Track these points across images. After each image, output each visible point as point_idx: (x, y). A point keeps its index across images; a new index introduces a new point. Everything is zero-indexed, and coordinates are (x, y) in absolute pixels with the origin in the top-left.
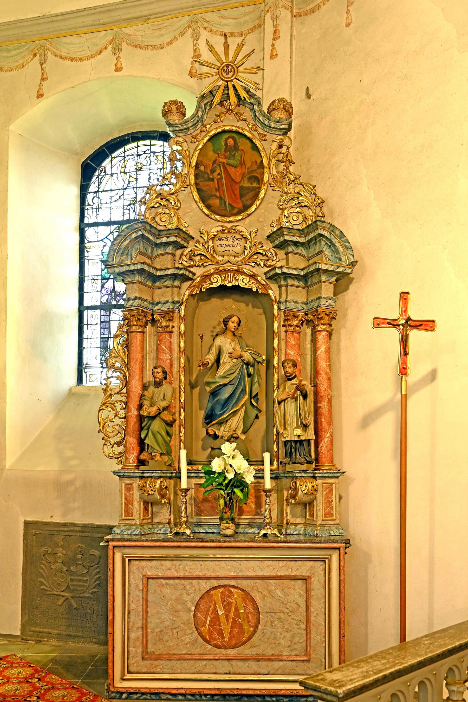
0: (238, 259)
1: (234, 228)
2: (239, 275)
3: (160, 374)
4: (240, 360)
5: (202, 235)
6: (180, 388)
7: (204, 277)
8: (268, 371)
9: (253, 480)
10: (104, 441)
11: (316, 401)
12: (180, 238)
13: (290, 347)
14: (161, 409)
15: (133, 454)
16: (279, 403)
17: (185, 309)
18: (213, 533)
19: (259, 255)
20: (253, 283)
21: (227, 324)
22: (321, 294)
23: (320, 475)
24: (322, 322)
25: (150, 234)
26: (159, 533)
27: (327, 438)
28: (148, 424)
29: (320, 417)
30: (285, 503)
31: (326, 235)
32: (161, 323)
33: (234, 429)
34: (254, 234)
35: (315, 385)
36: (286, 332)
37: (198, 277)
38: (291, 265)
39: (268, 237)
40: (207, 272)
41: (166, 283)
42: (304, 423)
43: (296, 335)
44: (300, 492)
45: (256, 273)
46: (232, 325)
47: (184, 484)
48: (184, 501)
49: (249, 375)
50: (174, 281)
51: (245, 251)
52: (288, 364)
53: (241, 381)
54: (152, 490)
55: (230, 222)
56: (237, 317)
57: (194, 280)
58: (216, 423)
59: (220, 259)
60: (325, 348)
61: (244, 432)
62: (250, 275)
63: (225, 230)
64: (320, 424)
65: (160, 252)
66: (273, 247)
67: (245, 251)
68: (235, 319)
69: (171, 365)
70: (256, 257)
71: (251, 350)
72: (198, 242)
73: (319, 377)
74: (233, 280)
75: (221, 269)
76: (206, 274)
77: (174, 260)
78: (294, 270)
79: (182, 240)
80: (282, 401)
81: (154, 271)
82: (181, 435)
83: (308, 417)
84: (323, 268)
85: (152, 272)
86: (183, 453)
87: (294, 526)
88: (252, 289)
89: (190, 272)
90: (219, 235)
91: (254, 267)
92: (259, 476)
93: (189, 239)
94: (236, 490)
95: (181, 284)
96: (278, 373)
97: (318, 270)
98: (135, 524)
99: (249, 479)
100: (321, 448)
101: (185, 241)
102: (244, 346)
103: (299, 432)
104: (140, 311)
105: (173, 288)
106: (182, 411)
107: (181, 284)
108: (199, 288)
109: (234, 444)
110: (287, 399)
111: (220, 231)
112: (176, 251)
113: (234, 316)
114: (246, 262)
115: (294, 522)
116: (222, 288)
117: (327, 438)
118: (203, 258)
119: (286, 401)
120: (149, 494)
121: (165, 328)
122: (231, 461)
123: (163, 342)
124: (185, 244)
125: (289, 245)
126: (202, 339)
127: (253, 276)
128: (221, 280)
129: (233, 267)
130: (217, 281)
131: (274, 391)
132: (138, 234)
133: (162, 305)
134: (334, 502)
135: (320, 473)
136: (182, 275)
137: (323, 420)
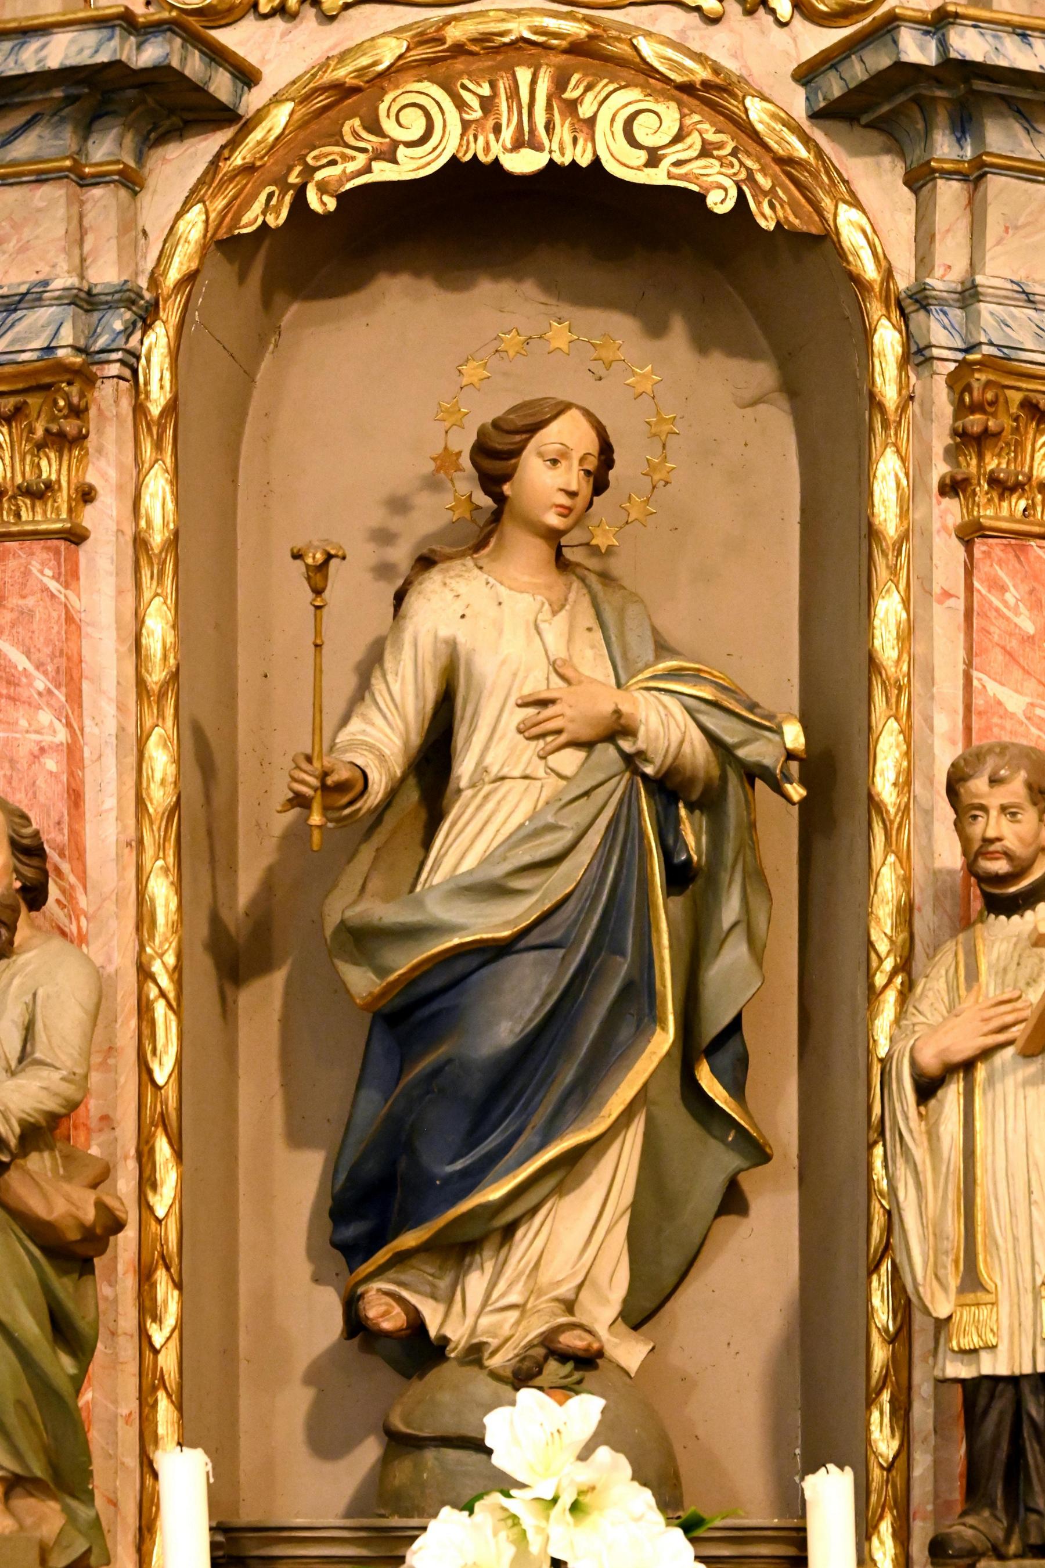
2: (603, 87)
4: (607, 754)
6: (144, 973)
7: (321, 101)
13: (997, 657)
16: (927, 1088)
17: (175, 354)
20: (706, 151)
21: (507, 477)
36: (971, 534)
37: (277, 100)
40: (343, 57)
41: (23, 148)
45: (731, 65)
46: (544, 479)
49: (680, 876)
50: (86, 128)
52: (995, 781)
56: (588, 414)
57: (248, 126)
61: (638, 1315)
62: (687, 88)
68: (570, 433)
71: (696, 677)
74: (549, 127)
75: (454, 34)
76: (342, 73)
86: (185, 1479)
88: (701, 198)
89: (218, 55)
95: (140, 158)
96: (905, 860)
102: (643, 648)
105: (85, 182)
106: (163, 1149)
107: (140, 158)
108: (285, 187)
109: (586, 1410)
110: (987, 1053)
113: (562, 408)
119: (981, 1072)
126: (318, 592)
127: (711, 95)
128: (455, 127)
129: (553, 24)
130: (421, 137)
131: (873, 995)
136: (162, 76)
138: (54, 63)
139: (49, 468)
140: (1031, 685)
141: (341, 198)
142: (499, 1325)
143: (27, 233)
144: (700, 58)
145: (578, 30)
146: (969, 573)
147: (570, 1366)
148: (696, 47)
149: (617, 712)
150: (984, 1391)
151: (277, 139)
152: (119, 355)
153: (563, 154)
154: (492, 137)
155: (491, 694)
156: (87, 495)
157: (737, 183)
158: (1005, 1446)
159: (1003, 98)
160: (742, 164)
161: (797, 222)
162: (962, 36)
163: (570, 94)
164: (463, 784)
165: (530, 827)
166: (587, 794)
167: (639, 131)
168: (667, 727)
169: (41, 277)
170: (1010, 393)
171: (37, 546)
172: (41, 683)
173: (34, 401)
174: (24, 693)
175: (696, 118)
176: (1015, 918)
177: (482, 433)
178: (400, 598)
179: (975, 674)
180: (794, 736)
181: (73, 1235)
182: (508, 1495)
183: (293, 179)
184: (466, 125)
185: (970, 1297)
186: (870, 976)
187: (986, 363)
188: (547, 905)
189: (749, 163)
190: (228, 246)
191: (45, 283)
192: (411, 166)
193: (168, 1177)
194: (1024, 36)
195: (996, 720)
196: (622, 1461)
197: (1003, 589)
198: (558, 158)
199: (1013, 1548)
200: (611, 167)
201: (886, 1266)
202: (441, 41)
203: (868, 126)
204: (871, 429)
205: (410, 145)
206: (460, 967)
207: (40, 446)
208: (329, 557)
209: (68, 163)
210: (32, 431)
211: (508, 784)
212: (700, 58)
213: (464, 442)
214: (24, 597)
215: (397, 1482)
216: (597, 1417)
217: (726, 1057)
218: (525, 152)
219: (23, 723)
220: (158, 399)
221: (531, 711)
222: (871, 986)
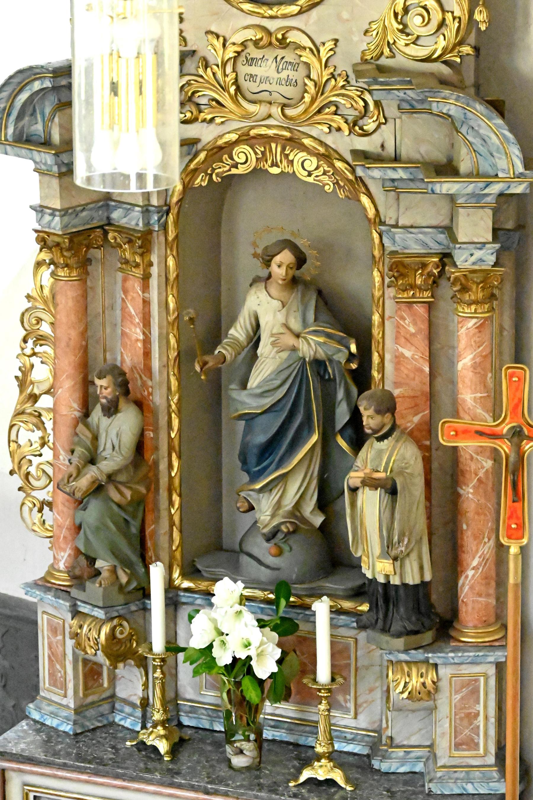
2: (296, 151)
3: (109, 390)
6: (170, 406)
8: (431, 313)
10: (22, 494)
13: (403, 340)
15: (64, 550)
27: (473, 568)
29: (459, 517)
51: (306, 95)
60: (473, 359)
64: (459, 534)
67: (306, 95)
69: (147, 354)
74: (281, 161)
76: (220, 142)
82: (173, 511)
90: (248, 51)
108: (207, 174)
117: (473, 568)
128: (254, 160)
134: (481, 718)
137: (465, 527)
140: (413, 348)
141: (222, 178)
145: (287, 134)
155: (264, 331)
156: (151, 264)
157: (334, 184)
160: (335, 178)
163: (287, 152)
167: (306, 164)
172: (137, 320)
175: (322, 162)
183: (209, 172)
184: (257, 159)
193: (176, 463)
195: (402, 359)
197: (404, 319)
202: (249, 135)
205: (241, 164)
218: (275, 168)
220: (170, 238)
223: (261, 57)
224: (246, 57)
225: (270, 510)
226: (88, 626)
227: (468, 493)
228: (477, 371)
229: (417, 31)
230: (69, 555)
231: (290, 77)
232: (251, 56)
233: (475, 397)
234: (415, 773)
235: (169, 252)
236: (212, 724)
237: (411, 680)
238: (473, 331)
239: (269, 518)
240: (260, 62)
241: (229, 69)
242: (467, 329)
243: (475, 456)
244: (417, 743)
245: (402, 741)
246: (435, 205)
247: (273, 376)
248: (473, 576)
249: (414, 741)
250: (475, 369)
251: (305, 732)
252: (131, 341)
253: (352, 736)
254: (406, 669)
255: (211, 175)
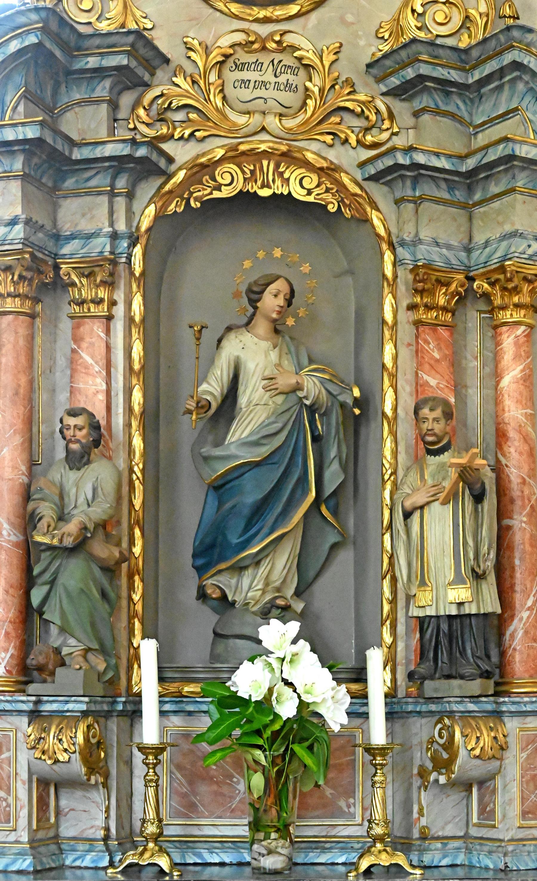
0: (290, 123)
1: (277, 38)
2: (292, 168)
3: (84, 431)
4: (293, 398)
5: (191, 54)
6: (131, 471)
7: (195, 170)
9: (345, 720)
11: (502, 513)
12: (136, 58)
13: (427, 367)
14: (91, 526)
17: (144, 255)
18: (222, 864)
19: (347, 116)
20: (327, 190)
21: (259, 300)
22: (513, 224)
23: (513, 708)
24: (516, 299)
25: (58, 44)
26: (80, 868)
27: (528, 609)
28: (53, 569)
30: (417, 782)
31: (531, 66)
32: (80, 290)
33: (277, 584)
34: (333, 57)
35: (498, 469)
36: (418, 323)
38: (430, 146)
39: (369, 66)
40: (204, 155)
41: (93, 183)
42: (477, 570)
43: (443, 332)
44: (462, 753)
45: (335, 161)
46: (271, 301)
47: (150, 731)
48: (151, 781)
49: (316, 439)
52: (431, 410)
53: (298, 451)
54: (66, 750)
55: (266, 20)
56: (287, 280)
57: (170, 177)
58: (227, 569)
59: (242, 120)
60: (522, 371)
61: (298, 593)
62: (321, 169)
63: (253, 43)
64: (508, 573)
65: (78, 96)
66: (383, 94)
67: (309, 101)
68: (279, 285)
70: (338, 120)
71: (323, 371)
72: (179, 70)
73: (505, 448)
74: (274, 181)
75: (242, 148)
76: (203, 160)
77: (115, 120)
78: (443, 159)
79: (140, 64)
80: (415, 509)
81: (66, 147)
83: (488, 554)
84: (523, 155)
85: (59, 147)
86: (148, 649)
87: (439, 845)
88: (325, 207)
89: (162, 153)
90: (237, 56)
91: (331, 146)
92: (358, 713)
93: (156, 62)
94: (297, 748)
97: (511, 157)
98: (17, 842)
99: (336, 717)
100: (512, 636)
101: (145, 68)
102: (305, 361)
103: (461, 593)
104: (27, 256)
106: (137, 532)
108: (183, 199)
109: (294, 627)
110: (428, 503)
111: (240, 44)
112: (120, 93)
113: (278, 278)
114: (308, 131)
115: (440, 834)
116: (245, 201)
118: (193, 116)
119: (426, 510)
120: (57, 761)
121: (92, 306)
122: (284, 670)
123: (84, 345)
124: (147, 77)
125: (427, 89)
126: (198, 339)
127: (329, 172)
128: (241, 180)
129: (276, 146)
130: (230, 182)
131: (384, 482)
132: (27, 43)
133: (83, 241)
135: (514, 703)
137: (517, 562)
138: (107, 154)
139: (102, 293)
140: (438, 376)
141: (202, 203)
142: (255, 596)
143: (94, 212)
144: (325, 159)
145: (284, 148)
146: (417, 337)
147: (280, 610)
148: (324, 155)
149: (297, 382)
150: (427, 620)
151: (181, 182)
152: (125, 255)
153: (278, 190)
154: (254, 184)
156: (113, 303)
157: (338, 202)
158: (434, 640)
159: (430, 176)
161: (358, 216)
162: (417, 155)
164: (243, 406)
165: (267, 422)
166: (288, 410)
167: (305, 183)
168: (312, 387)
169: (99, 227)
170: (432, 277)
171: (96, 320)
172: (97, 369)
173: (97, 269)
174: (91, 371)
176: (437, 457)
177: (250, 285)
178: (220, 341)
179: (419, 372)
180: (356, 393)
181: (113, 563)
182: (268, 657)
184: (245, 179)
185: (423, 589)
186: (383, 475)
187: (424, 266)
188: (273, 449)
189: (342, 195)
190: (158, 218)
191: (101, 229)
192: (225, 193)
194: (438, 156)
196: (307, 644)
197: (429, 343)
198: (276, 192)
199: (437, 675)
200: (295, 195)
201: (388, 577)
202: (237, 150)
203: (383, 184)
204: (383, 287)
205: (225, 185)
206: (242, 470)
207: (98, 286)
208: (202, 327)
209: (109, 188)
210: (96, 281)
211: (259, 407)
212: (325, 159)
213: (243, 288)
214: (91, 338)
215: (218, 651)
216: (298, 629)
217: (332, 503)
218: (265, 189)
219: (91, 382)
221: (266, 381)
222: (383, 479)
223: (255, 61)
224: (234, 62)
225: (262, 582)
226: (57, 726)
227: (522, 522)
228: (527, 384)
229: (436, 30)
230: (12, 655)
231: (290, 82)
232: (241, 61)
233: (526, 413)
234: (457, 865)
235: (134, 286)
236: (183, 857)
237: (481, 733)
238: (522, 340)
239: (260, 593)
240: (253, 66)
241: (213, 77)
242: (516, 337)
243: (527, 479)
244: (450, 834)
245: (437, 832)
246: (455, 220)
247: (272, 419)
248: (528, 617)
249: (449, 831)
250: (524, 381)
251: (302, 849)
252: (87, 396)
253: (360, 845)
254: (474, 724)
255: (188, 200)
